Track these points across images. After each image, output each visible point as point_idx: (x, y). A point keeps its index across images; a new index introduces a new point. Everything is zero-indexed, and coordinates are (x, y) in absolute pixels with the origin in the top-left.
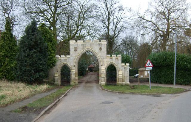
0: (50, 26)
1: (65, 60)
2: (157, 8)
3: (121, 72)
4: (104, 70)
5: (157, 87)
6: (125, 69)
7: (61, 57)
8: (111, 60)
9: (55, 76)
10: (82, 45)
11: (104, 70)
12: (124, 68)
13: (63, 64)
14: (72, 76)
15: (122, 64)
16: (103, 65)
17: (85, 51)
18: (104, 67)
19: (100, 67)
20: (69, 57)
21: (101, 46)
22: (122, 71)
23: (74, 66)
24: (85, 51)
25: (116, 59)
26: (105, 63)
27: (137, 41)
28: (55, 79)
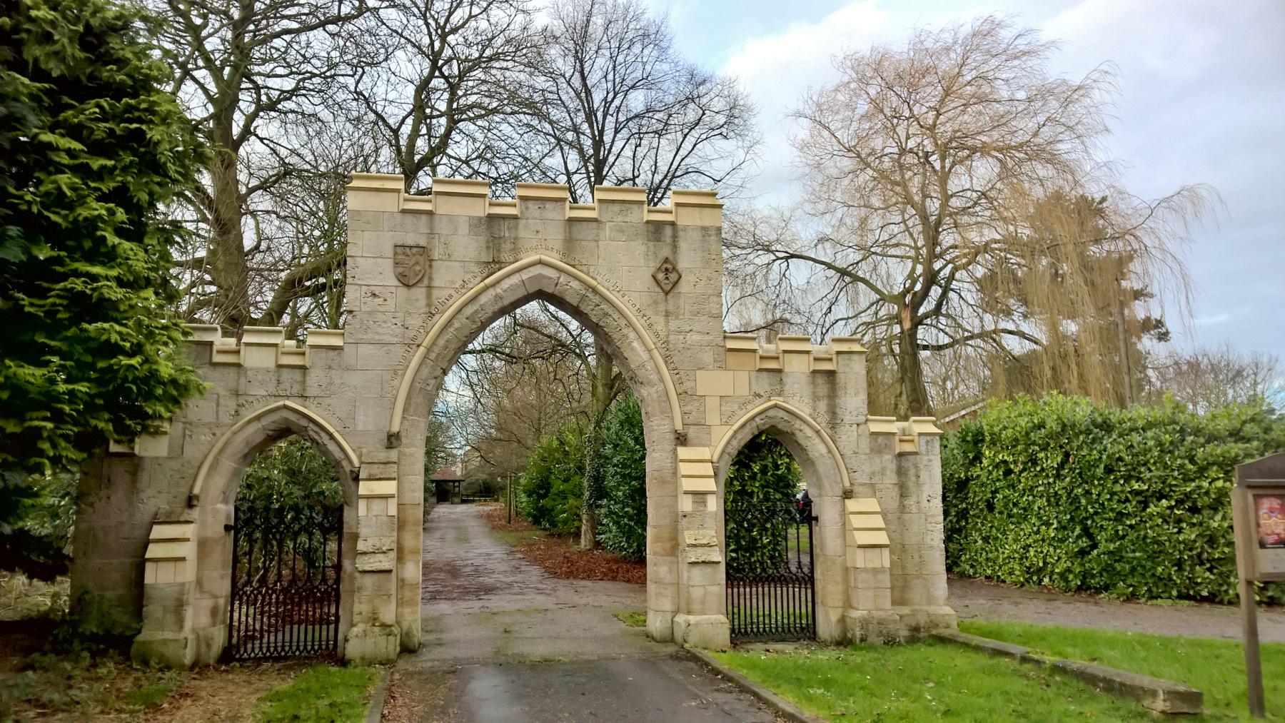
0: (104, 135)
1: (285, 374)
2: (890, 79)
3: (872, 504)
4: (710, 485)
5: (520, 600)
6: (900, 472)
7: (246, 339)
8: (764, 385)
9: (153, 551)
10: (476, 223)
11: (710, 485)
12: (892, 466)
13: (266, 421)
14: (361, 546)
15: (875, 427)
16: (692, 433)
17: (506, 284)
18: (704, 453)
19: (655, 461)
20: (337, 341)
21: (675, 247)
22: (873, 489)
23: (392, 440)
24: (506, 284)
25: (820, 380)
26: (712, 418)
27: (143, 491)
28: (147, 590)
